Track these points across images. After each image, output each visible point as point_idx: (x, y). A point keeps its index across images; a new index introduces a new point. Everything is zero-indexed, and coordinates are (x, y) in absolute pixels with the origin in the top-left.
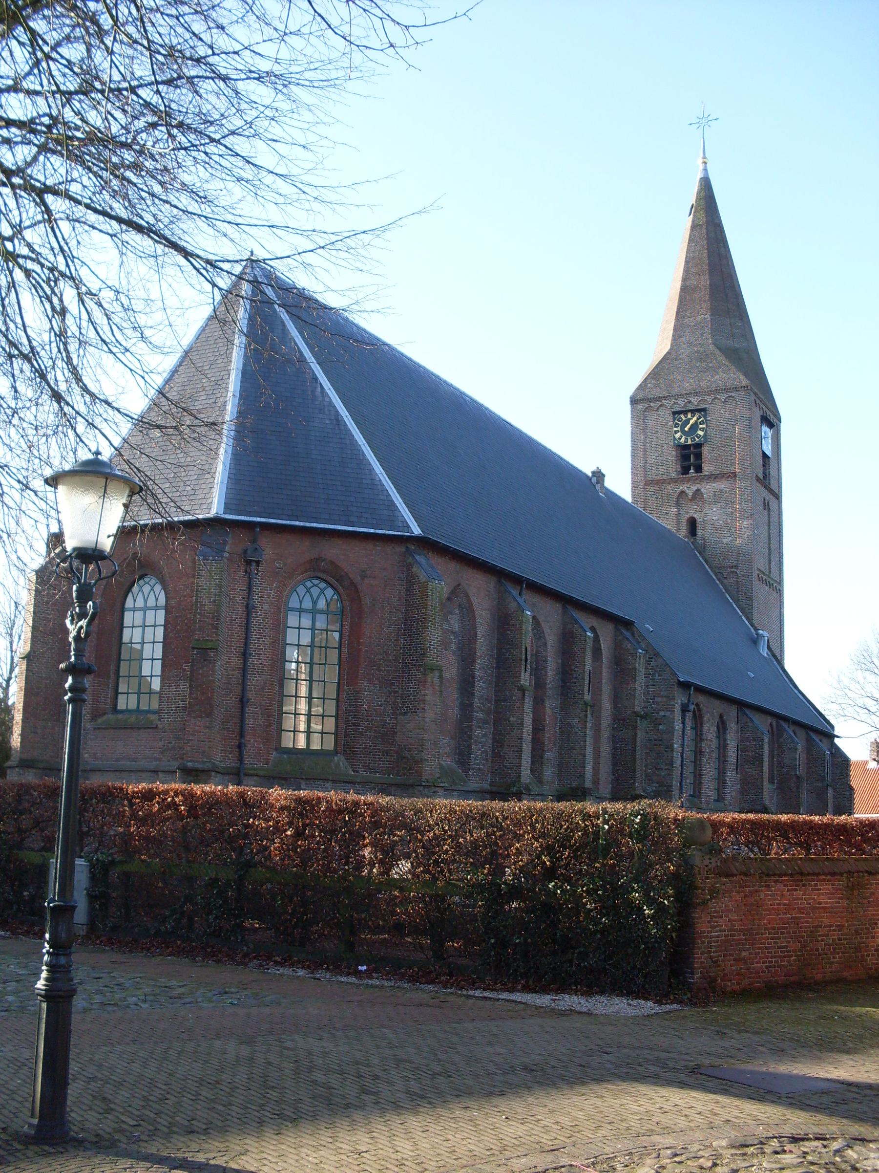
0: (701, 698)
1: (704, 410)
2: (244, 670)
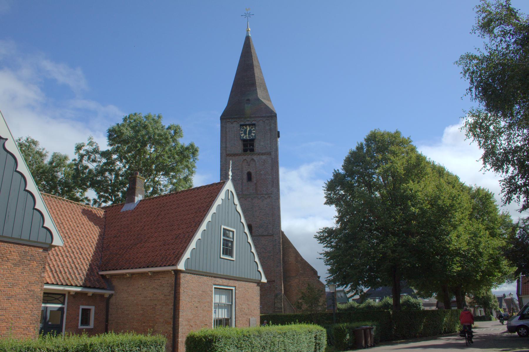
1: (254, 125)
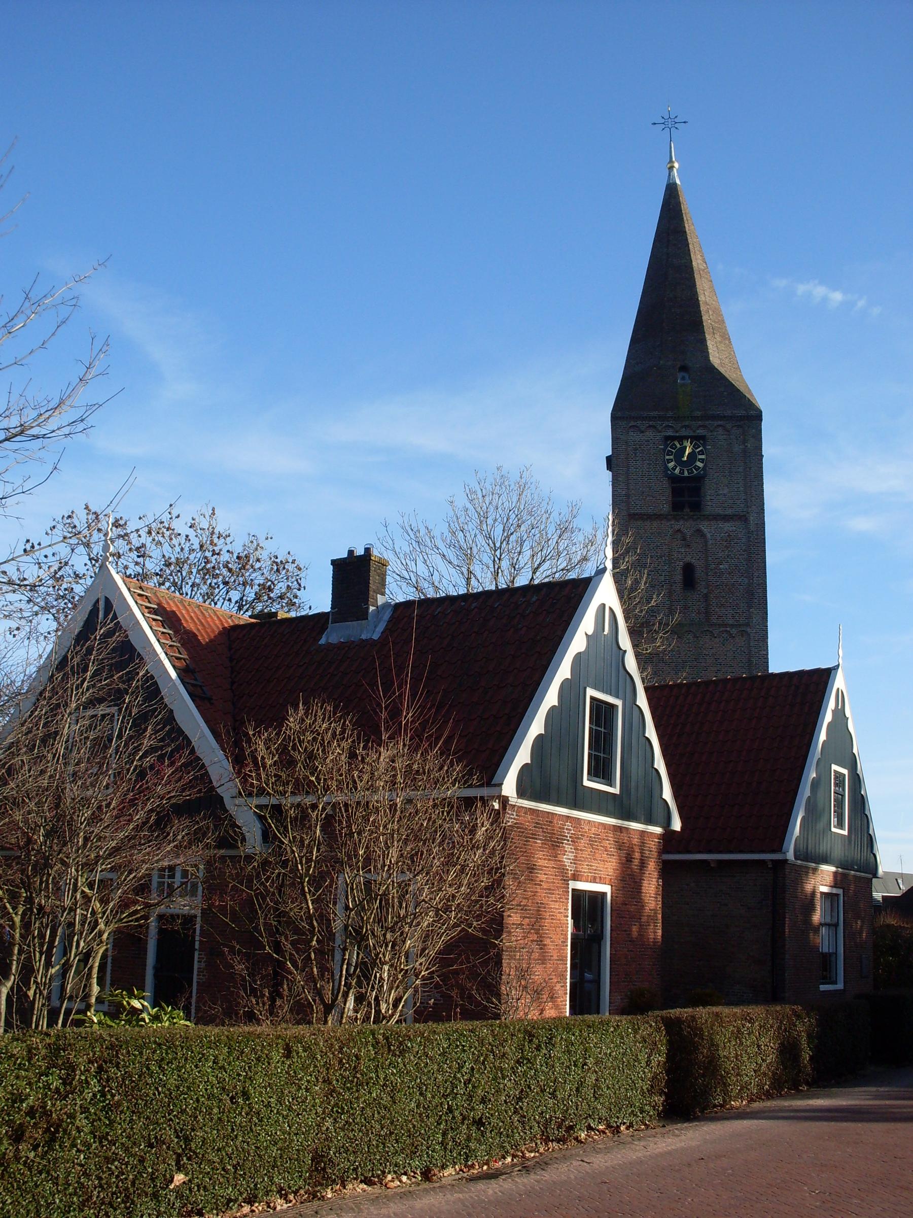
1: (703, 438)
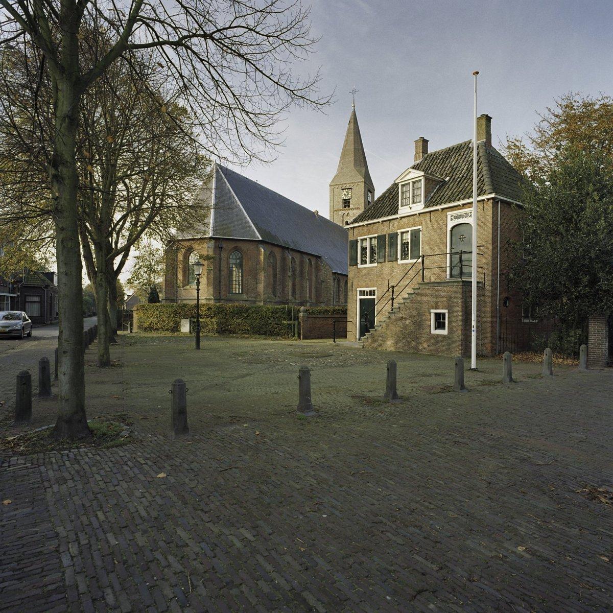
0: (340, 276)
1: (351, 188)
2: (220, 274)
